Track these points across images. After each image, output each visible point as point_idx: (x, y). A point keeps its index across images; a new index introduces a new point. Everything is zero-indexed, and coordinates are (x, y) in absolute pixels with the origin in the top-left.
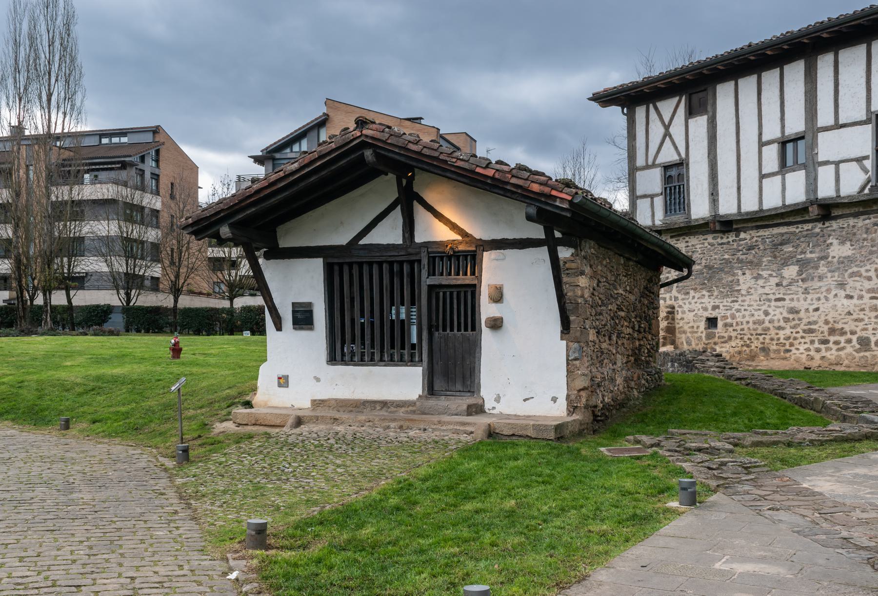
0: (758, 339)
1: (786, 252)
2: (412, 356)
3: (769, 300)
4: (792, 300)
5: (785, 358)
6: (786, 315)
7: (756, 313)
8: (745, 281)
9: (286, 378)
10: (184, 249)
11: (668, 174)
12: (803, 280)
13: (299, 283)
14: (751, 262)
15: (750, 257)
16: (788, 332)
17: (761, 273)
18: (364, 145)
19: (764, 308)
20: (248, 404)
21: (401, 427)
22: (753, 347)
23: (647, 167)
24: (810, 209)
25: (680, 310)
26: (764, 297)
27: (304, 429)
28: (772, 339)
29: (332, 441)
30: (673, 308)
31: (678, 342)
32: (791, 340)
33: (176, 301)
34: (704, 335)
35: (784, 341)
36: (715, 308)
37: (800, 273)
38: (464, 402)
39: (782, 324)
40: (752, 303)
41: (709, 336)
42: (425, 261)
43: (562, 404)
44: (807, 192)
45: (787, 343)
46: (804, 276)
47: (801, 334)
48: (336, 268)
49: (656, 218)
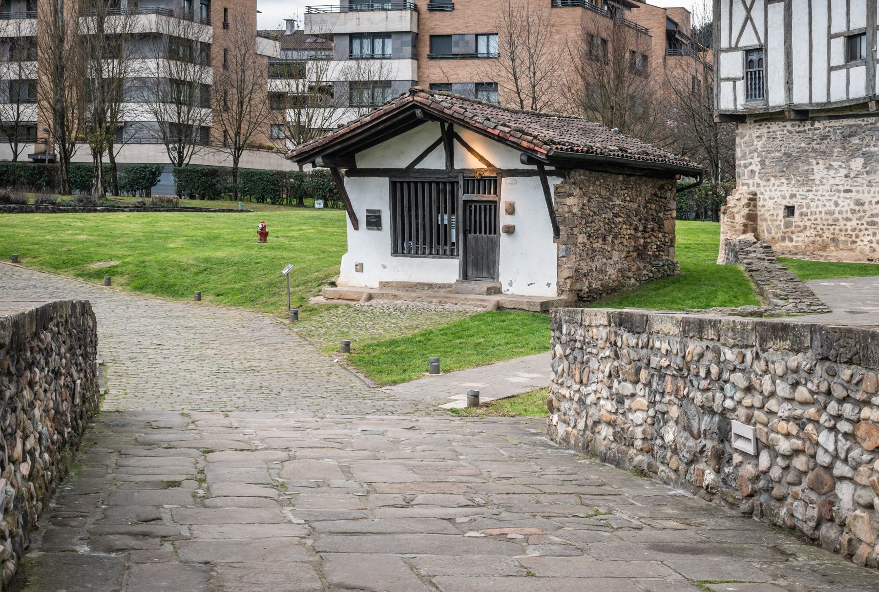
0: (829, 229)
1: (854, 144)
2: (452, 251)
3: (839, 191)
4: (858, 192)
5: (852, 250)
6: (853, 206)
7: (827, 204)
8: (819, 170)
9: (362, 265)
10: (247, 100)
11: (750, 58)
12: (867, 173)
13: (370, 195)
14: (824, 152)
15: (823, 147)
16: (854, 223)
17: (832, 163)
18: (415, 106)
19: (834, 198)
20: (333, 284)
21: (440, 302)
22: (825, 238)
23: (730, 49)
24: (870, 104)
25: (761, 197)
26: (835, 188)
27: (373, 302)
28: (841, 230)
29: (392, 310)
30: (756, 194)
31: (759, 229)
32: (857, 232)
33: (236, 162)
34: (782, 224)
35: (851, 233)
36: (793, 196)
37: (865, 165)
38: (484, 285)
39: (849, 215)
40: (824, 193)
41: (788, 225)
42: (461, 183)
43: (554, 287)
44: (867, 88)
45: (854, 234)
46: (868, 169)
47: (865, 226)
48: (398, 185)
49: (738, 103)
